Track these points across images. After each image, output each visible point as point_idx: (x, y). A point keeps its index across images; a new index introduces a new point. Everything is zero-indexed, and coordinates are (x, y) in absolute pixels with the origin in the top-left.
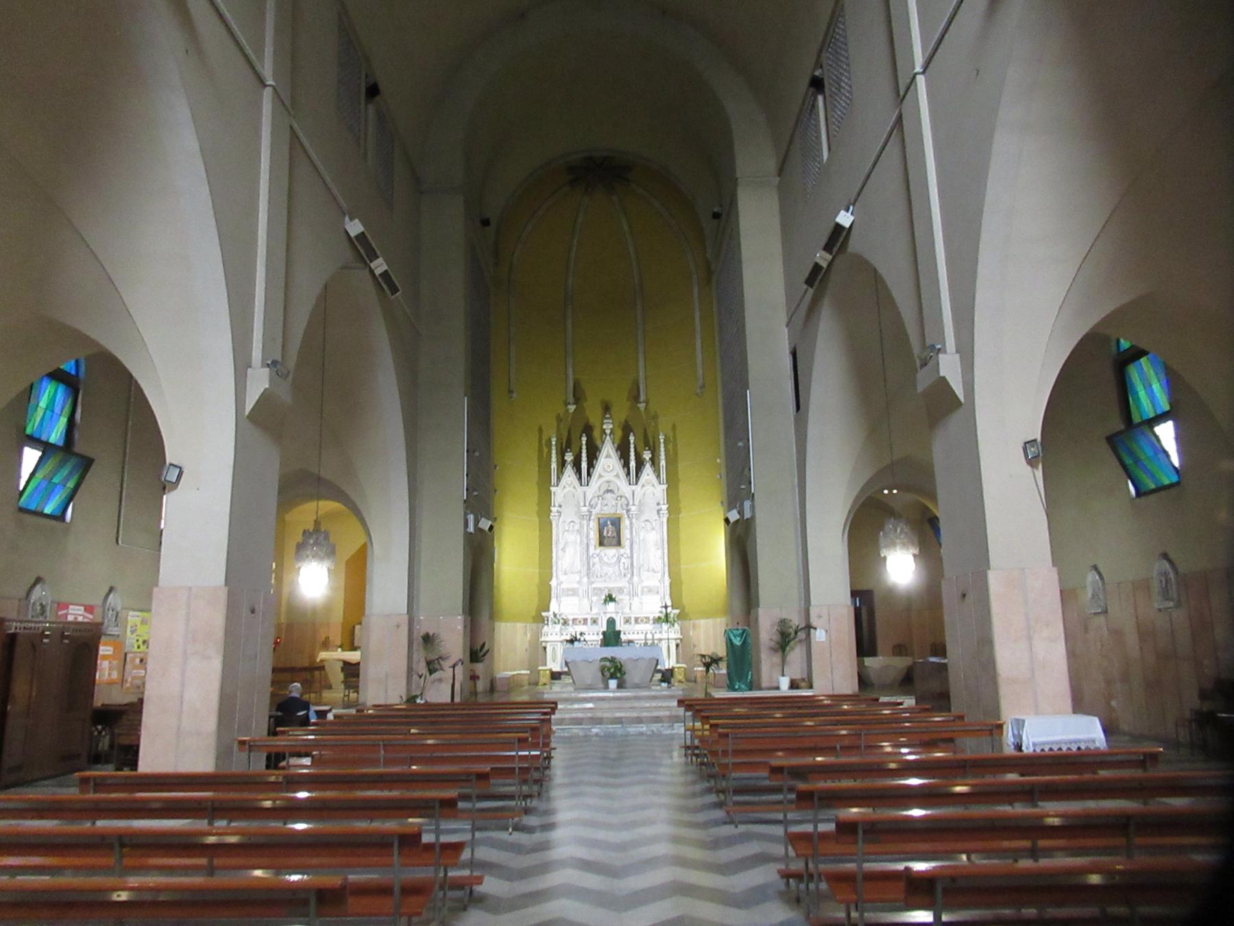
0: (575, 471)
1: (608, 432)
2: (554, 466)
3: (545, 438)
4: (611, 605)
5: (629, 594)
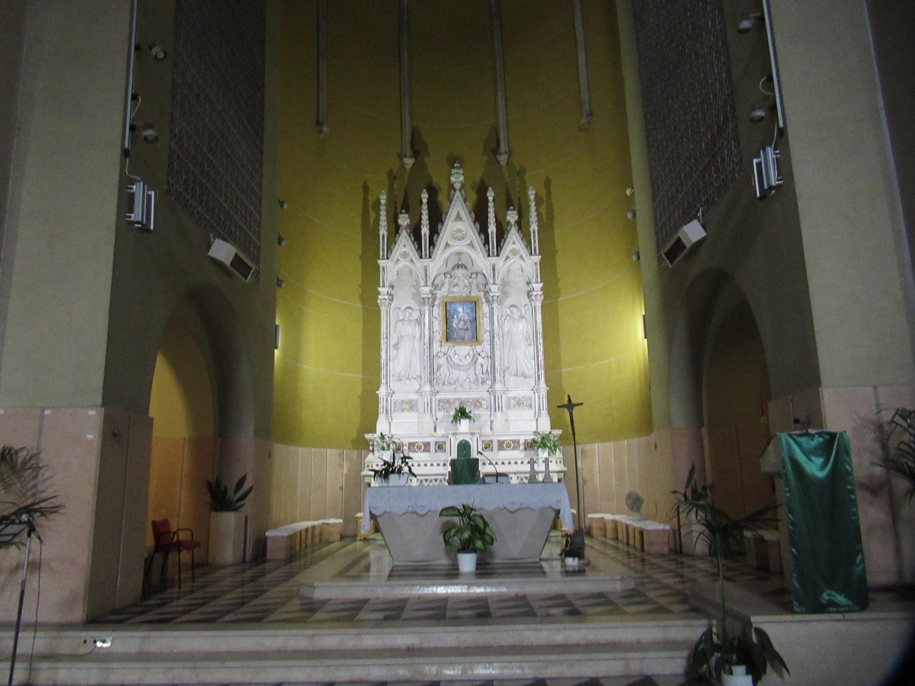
0: (413, 239)
2: (383, 231)
3: (371, 199)
4: (465, 423)
5: (489, 408)
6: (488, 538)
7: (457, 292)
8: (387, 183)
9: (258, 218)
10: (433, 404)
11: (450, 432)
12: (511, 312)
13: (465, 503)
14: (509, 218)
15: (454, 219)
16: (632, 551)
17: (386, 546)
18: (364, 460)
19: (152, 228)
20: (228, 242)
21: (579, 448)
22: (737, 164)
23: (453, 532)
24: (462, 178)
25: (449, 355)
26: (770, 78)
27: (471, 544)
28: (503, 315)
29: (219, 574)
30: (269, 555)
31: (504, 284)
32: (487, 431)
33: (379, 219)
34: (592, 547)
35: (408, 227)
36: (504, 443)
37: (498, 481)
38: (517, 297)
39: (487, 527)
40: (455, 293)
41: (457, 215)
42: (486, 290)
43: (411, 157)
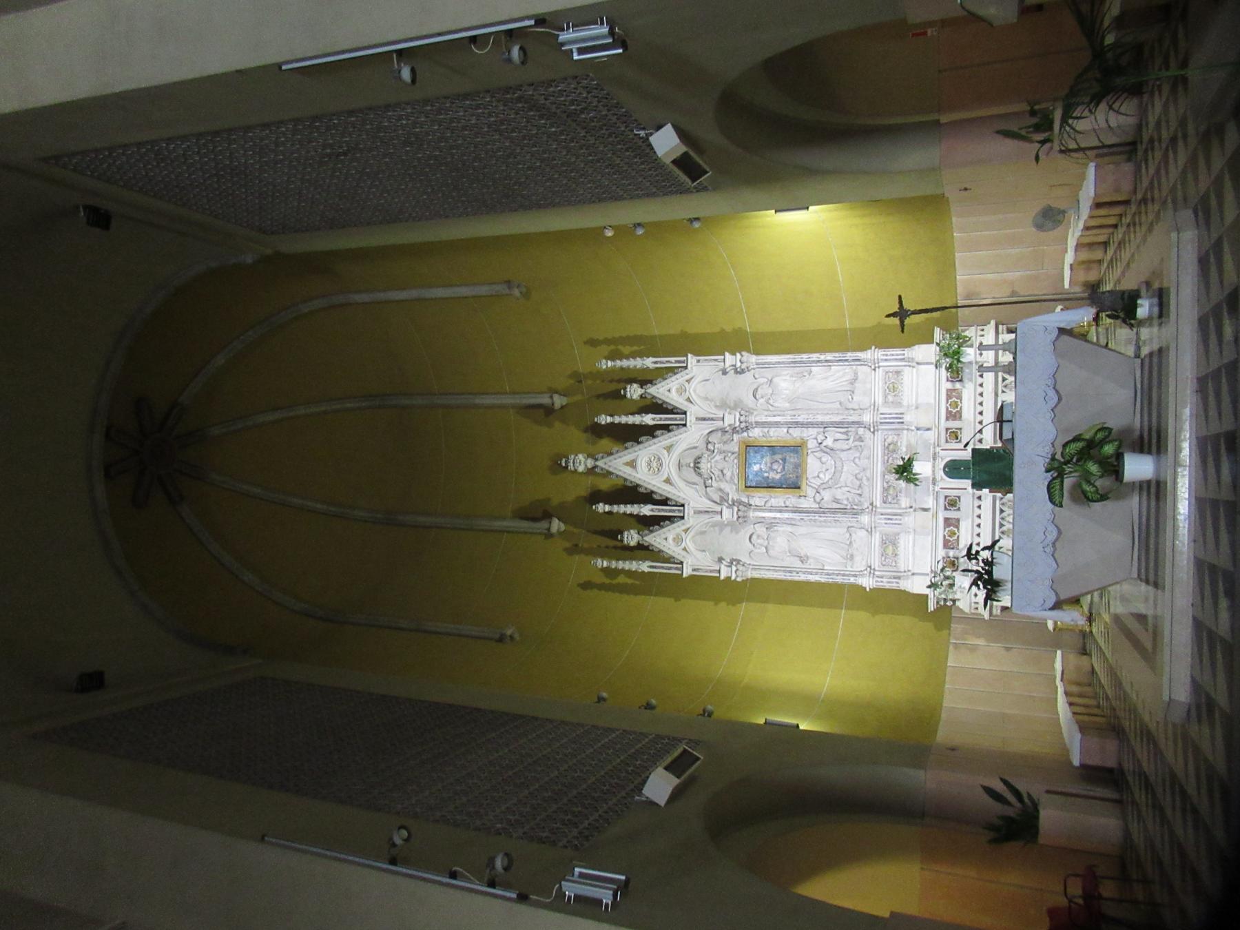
0: (656, 527)
1: (590, 463)
2: (645, 567)
4: (918, 467)
5: (898, 433)
6: (1100, 436)
7: (731, 469)
8: (583, 556)
9: (617, 733)
10: (889, 511)
11: (931, 488)
12: (762, 397)
13: (1044, 469)
14: (636, 396)
15: (634, 471)
16: (1127, 220)
17: (1103, 590)
18: (967, 614)
19: (623, 878)
20: (648, 777)
21: (960, 303)
22: (578, 83)
23: (1087, 488)
24: (581, 457)
25: (819, 486)
26: (473, 39)
27: (1109, 460)
28: (767, 409)
29: (1138, 838)
30: (1111, 763)
31: (723, 405)
32: (931, 436)
33: (628, 570)
34: (1118, 281)
35: (641, 533)
36: (951, 412)
37: (1010, 419)
38: (741, 388)
39: (1082, 437)
40: (733, 474)
41: (627, 465)
42: (730, 431)
43: (550, 523)
